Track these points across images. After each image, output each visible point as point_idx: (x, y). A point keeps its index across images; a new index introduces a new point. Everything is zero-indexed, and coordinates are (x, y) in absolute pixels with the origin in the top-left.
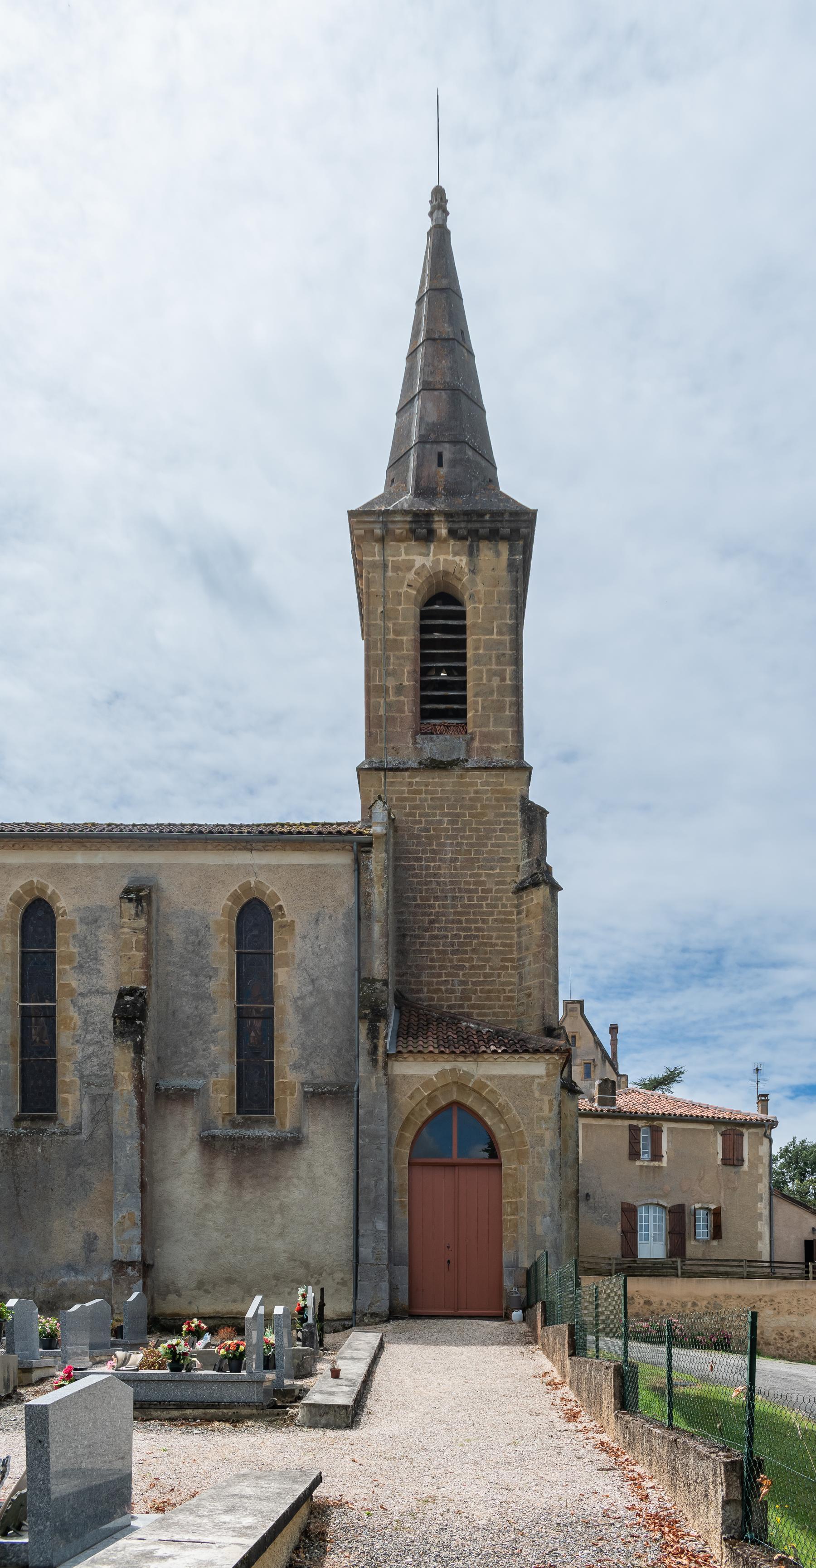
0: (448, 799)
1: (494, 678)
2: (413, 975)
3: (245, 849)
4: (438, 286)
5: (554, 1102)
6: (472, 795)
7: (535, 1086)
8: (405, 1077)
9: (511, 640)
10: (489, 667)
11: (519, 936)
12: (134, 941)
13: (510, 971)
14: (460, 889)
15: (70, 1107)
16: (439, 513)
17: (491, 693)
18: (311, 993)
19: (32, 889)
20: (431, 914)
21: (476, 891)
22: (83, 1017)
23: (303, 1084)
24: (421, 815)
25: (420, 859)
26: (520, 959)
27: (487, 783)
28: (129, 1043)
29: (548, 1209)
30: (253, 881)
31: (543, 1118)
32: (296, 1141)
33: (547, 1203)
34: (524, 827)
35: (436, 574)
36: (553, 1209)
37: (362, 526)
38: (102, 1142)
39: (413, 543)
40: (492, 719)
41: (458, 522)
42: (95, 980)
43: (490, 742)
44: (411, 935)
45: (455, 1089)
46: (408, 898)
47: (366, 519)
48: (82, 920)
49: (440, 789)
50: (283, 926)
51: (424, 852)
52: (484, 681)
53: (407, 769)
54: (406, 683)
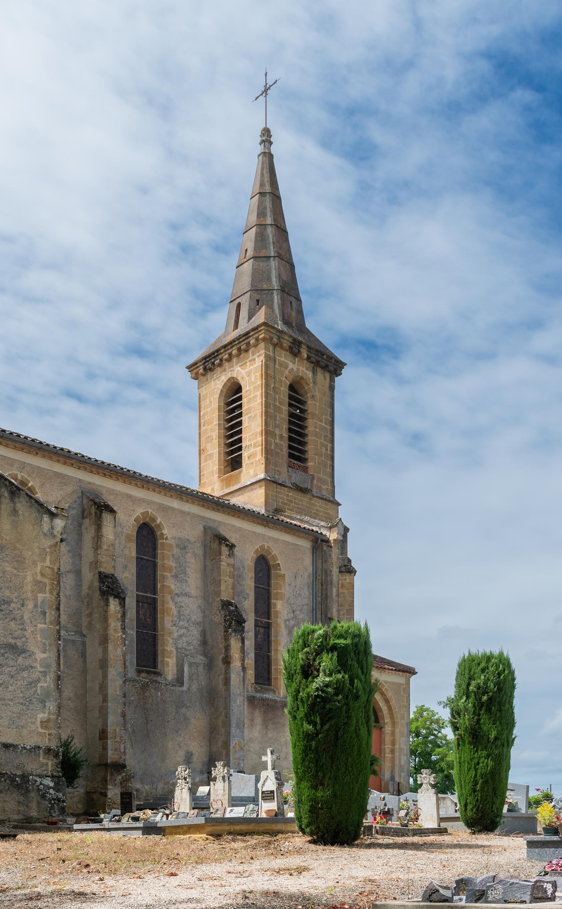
3: (263, 525)
7: (401, 689)
12: (228, 571)
15: (170, 668)
16: (305, 344)
22: (178, 609)
27: (321, 507)
33: (405, 749)
38: (195, 694)
39: (288, 353)
42: (184, 587)
48: (177, 546)
52: (319, 448)
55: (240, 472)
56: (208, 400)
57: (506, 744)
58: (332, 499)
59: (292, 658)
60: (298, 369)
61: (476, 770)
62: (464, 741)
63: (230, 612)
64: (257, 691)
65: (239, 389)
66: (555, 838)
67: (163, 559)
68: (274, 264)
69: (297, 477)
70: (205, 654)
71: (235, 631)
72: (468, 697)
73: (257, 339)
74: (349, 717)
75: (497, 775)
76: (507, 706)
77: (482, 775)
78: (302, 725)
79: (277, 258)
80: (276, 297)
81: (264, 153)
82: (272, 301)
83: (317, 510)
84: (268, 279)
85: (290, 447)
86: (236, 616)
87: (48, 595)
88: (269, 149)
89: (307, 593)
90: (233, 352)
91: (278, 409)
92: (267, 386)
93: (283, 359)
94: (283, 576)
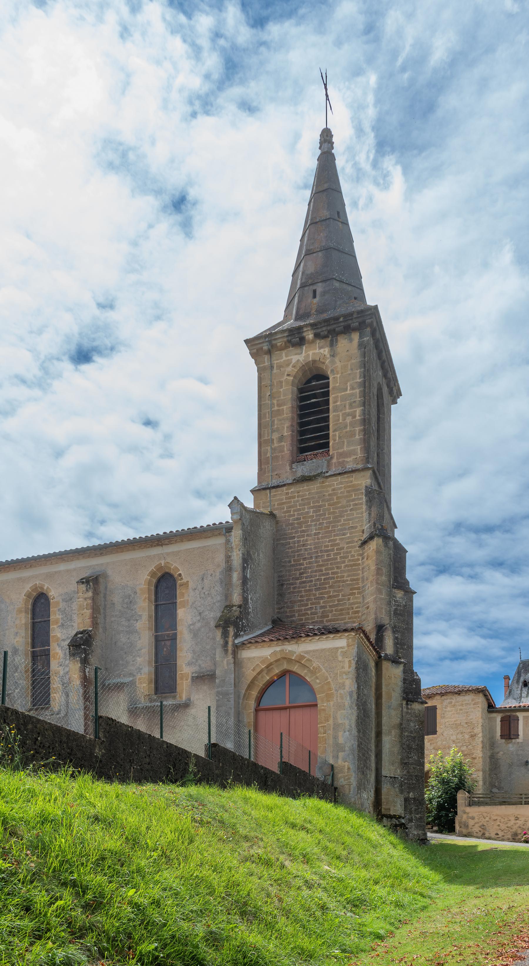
0: (313, 498)
1: (347, 418)
2: (288, 607)
3: (158, 545)
4: (321, 189)
5: (352, 662)
6: (330, 492)
8: (249, 659)
9: (360, 391)
10: (344, 412)
11: (363, 573)
12: (85, 605)
13: (356, 596)
14: (321, 551)
17: (346, 427)
18: (199, 621)
19: (36, 588)
20: (301, 569)
21: (333, 550)
22: (64, 652)
23: (193, 673)
24: (294, 511)
25: (294, 537)
26: (363, 587)
27: (341, 483)
28: (78, 659)
29: (347, 727)
31: (344, 673)
32: (186, 705)
33: (347, 724)
34: (367, 505)
35: (307, 364)
36: (351, 727)
37: (255, 347)
39: (291, 349)
40: (346, 443)
41: (321, 327)
42: (70, 631)
43: (344, 458)
44: (288, 584)
45: (285, 663)
46: (285, 562)
47: (257, 342)
48: (64, 600)
49: (307, 493)
50: (181, 585)
51: (296, 532)
53: (284, 485)
54: (286, 434)
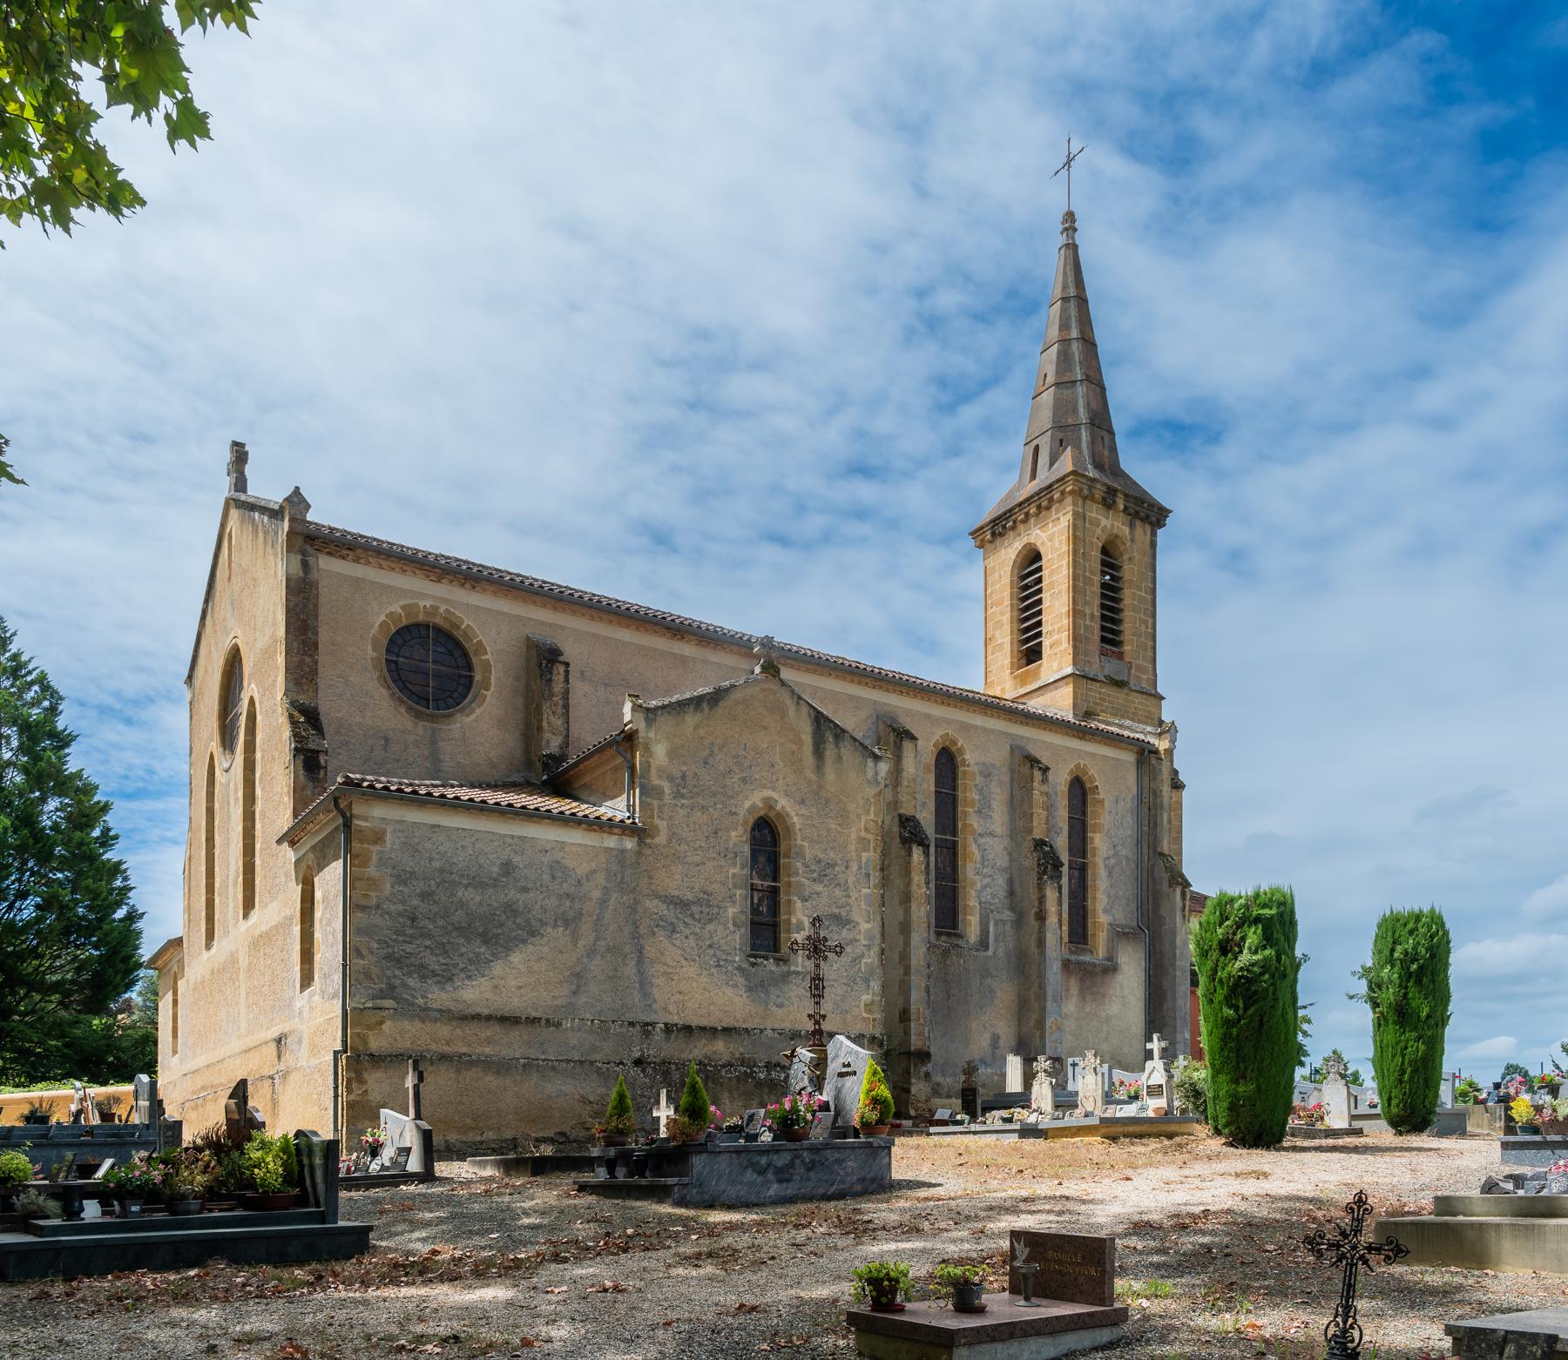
27: (1140, 703)
30: (1082, 762)
48: (980, 772)
55: (1040, 666)
56: (996, 574)
57: (1440, 1024)
58: (1153, 692)
59: (1206, 932)
60: (1113, 525)
61: (1403, 1056)
62: (1386, 1020)
63: (1046, 854)
64: (1071, 952)
65: (1037, 557)
66: (1537, 1138)
67: (965, 791)
68: (1081, 390)
69: (1111, 667)
70: (1012, 909)
71: (1051, 878)
72: (1393, 966)
73: (1063, 493)
74: (1276, 999)
75: (1430, 1063)
76: (1442, 976)
77: (1410, 1062)
78: (1221, 1009)
79: (1085, 382)
80: (1084, 434)
81: (1067, 245)
82: (1080, 439)
83: (1135, 708)
84: (1074, 410)
85: (1103, 628)
86: (1053, 859)
87: (872, 853)
88: (1073, 238)
89: (1131, 822)
90: (1031, 511)
91: (1089, 581)
92: (1075, 552)
93: (1094, 515)
94: (1102, 801)
